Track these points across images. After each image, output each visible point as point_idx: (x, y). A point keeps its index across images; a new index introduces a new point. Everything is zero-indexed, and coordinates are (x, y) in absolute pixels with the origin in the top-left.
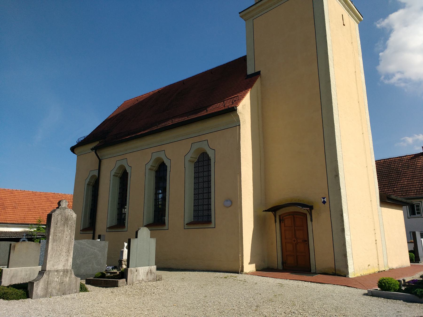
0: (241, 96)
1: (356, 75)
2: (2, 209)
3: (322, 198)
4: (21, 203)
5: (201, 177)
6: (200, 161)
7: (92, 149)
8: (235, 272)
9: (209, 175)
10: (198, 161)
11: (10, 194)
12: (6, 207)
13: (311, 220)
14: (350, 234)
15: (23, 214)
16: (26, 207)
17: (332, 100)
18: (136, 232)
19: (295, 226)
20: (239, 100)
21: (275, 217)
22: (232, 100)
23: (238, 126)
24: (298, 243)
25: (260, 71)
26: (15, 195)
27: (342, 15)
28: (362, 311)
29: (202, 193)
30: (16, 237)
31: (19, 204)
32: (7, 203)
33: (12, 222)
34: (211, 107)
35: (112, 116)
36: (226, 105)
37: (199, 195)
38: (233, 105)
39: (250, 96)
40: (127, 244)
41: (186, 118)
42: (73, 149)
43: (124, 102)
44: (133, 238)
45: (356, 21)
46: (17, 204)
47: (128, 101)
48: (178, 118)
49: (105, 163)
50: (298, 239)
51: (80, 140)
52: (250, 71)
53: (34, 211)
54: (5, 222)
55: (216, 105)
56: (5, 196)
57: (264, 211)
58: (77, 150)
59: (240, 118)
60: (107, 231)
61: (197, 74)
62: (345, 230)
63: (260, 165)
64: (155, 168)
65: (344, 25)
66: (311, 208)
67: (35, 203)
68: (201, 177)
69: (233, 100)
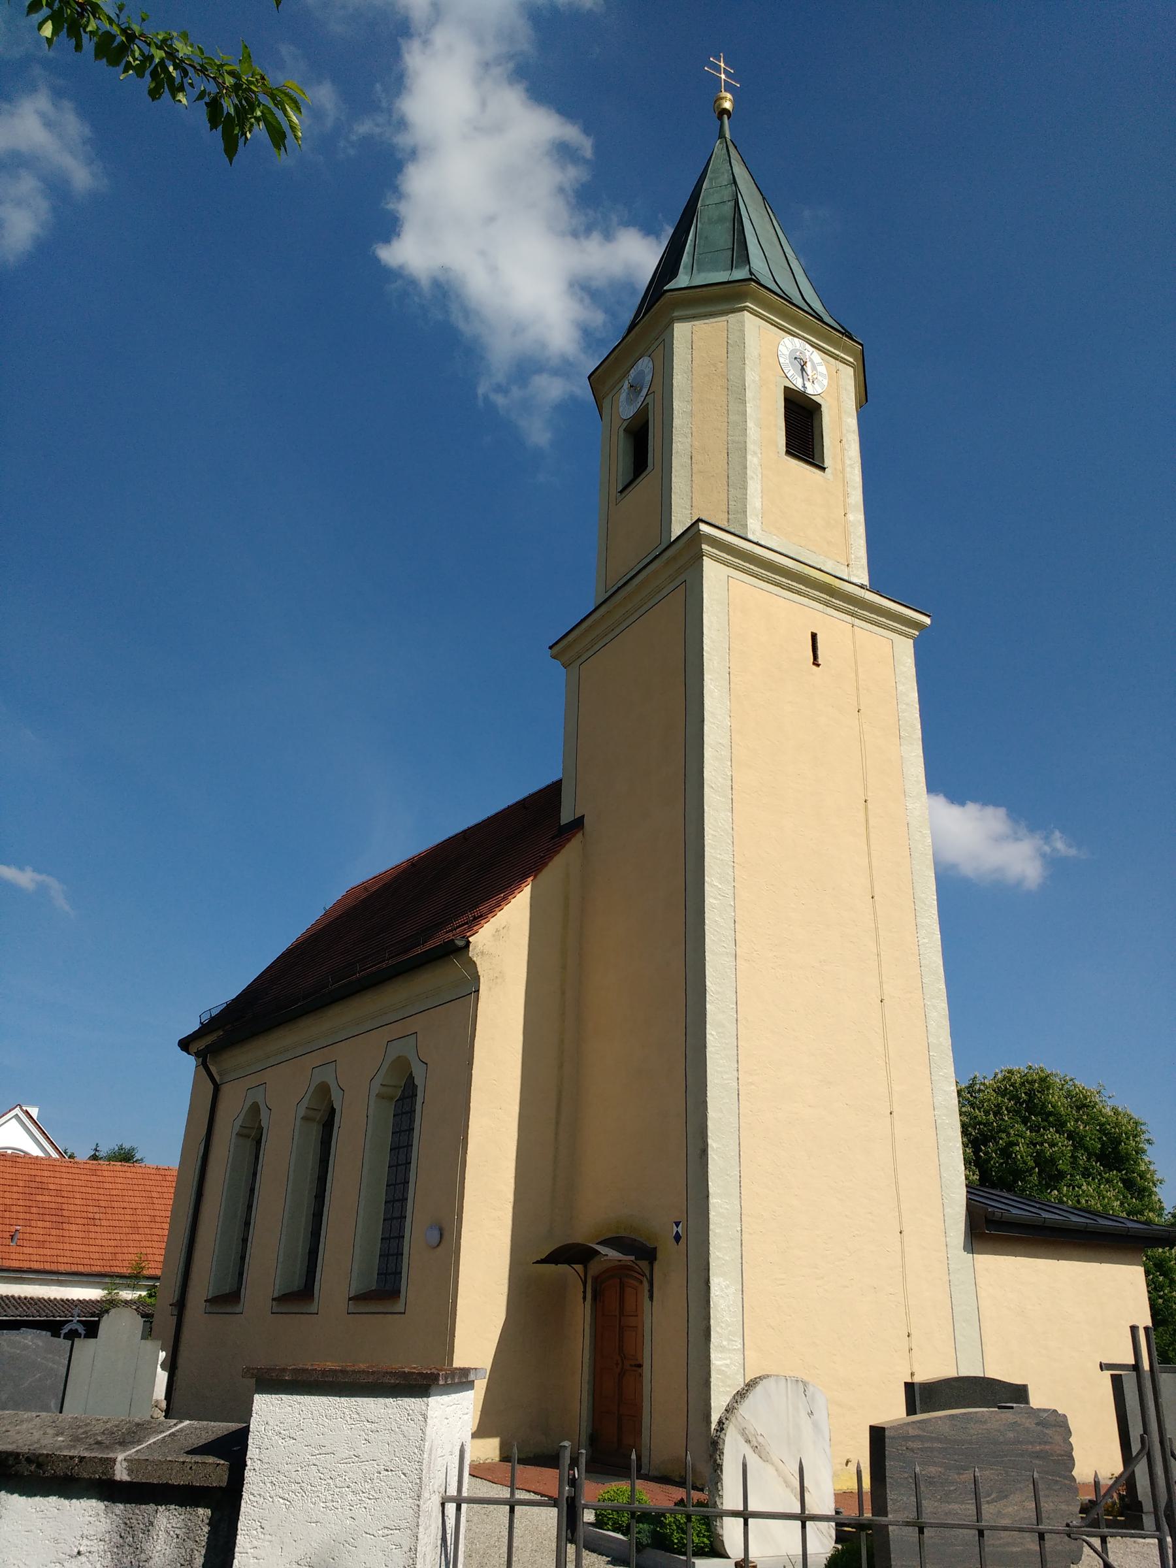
2: (54, 1225)
3: (675, 1222)
4: (115, 1204)
5: (404, 1147)
8: (1155, 1495)
11: (88, 1178)
12: (66, 1220)
13: (651, 1298)
14: (740, 1346)
15: (113, 1243)
16: (128, 1217)
17: (704, 913)
21: (585, 1284)
26: (101, 1179)
27: (814, 636)
28: (89, 1550)
30: (66, 1317)
31: (109, 1210)
32: (72, 1207)
33: (74, 1268)
39: (531, 897)
40: (164, 1353)
43: (347, 892)
45: (901, 633)
46: (103, 1210)
52: (566, 817)
53: (148, 1231)
54: (54, 1267)
56: (71, 1182)
59: (479, 969)
60: (207, 1311)
65: (818, 665)
66: (648, 1254)
67: (158, 1207)
69: (470, 916)
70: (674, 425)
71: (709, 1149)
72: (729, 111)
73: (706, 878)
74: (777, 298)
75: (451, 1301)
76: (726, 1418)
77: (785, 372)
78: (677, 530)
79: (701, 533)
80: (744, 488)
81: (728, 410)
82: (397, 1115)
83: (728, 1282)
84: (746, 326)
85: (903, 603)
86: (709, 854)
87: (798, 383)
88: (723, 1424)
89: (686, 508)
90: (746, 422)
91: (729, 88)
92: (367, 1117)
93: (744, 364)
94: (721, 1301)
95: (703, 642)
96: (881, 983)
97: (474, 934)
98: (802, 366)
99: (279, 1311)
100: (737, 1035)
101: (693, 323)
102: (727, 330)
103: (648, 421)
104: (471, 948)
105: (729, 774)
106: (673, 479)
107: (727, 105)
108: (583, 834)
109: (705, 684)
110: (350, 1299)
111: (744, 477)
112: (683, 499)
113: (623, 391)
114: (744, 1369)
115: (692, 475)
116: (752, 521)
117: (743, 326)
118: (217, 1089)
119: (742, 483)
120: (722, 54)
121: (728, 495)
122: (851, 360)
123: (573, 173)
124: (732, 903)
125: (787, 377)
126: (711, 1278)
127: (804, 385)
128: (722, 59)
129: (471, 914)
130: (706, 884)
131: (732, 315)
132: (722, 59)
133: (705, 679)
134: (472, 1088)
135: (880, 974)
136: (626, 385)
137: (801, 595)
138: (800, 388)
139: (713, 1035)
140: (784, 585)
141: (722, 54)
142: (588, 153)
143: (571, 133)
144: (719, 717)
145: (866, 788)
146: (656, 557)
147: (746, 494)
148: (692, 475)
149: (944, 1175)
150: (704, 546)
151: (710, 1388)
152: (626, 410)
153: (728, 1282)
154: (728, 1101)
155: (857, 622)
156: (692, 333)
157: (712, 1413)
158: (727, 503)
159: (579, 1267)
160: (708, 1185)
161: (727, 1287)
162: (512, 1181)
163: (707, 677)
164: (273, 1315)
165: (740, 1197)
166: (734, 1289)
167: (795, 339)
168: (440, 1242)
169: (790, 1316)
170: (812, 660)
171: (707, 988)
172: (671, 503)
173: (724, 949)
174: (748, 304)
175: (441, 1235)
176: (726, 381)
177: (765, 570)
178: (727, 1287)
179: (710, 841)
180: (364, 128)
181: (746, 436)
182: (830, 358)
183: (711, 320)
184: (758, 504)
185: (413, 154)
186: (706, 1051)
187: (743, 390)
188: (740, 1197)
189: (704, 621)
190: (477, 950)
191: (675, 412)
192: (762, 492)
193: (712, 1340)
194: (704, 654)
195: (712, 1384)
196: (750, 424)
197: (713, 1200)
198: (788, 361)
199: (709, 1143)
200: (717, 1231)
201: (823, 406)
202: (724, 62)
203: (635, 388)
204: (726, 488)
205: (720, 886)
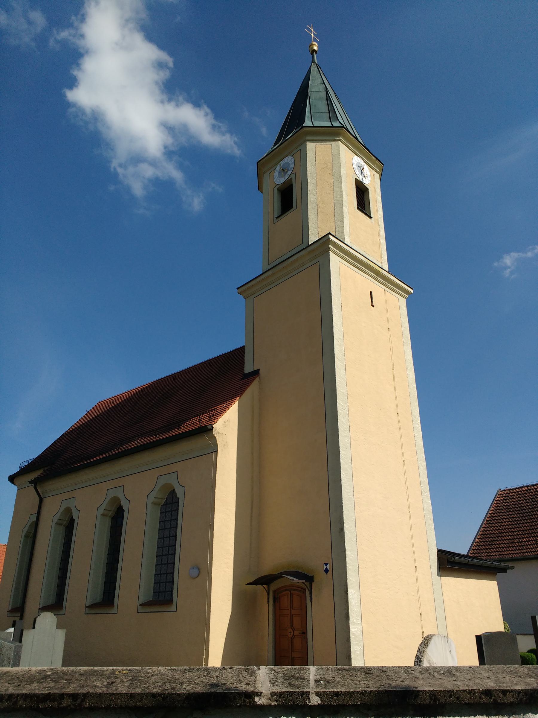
0: (225, 407)
1: (393, 373)
3: (324, 564)
5: (168, 528)
6: (168, 503)
7: (31, 482)
9: (171, 527)
10: (166, 504)
13: (311, 600)
14: (361, 622)
18: (34, 619)
19: (292, 609)
20: (218, 415)
21: (268, 594)
22: (200, 417)
23: (215, 452)
24: (295, 636)
25: (259, 369)
27: (371, 293)
29: (167, 555)
34: (183, 425)
35: (78, 425)
36: (202, 420)
37: (169, 557)
38: (210, 421)
41: (154, 439)
42: (12, 479)
43: (97, 403)
44: (29, 628)
45: (402, 296)
47: (116, 396)
48: (140, 439)
49: (47, 502)
50: (295, 630)
51: (23, 465)
52: (248, 369)
55: (194, 419)
57: (248, 584)
58: (17, 480)
59: (217, 441)
61: (194, 364)
62: (350, 616)
63: (252, 508)
64: (110, 514)
65: (373, 306)
66: (310, 579)
68: (168, 528)
69: (211, 415)
70: (308, 189)
71: (345, 528)
72: (316, 51)
73: (337, 400)
74: (352, 137)
75: (207, 604)
76: (421, 656)
77: (356, 171)
78: (313, 239)
79: (330, 239)
80: (343, 222)
81: (333, 185)
82: (162, 513)
83: (355, 592)
84: (340, 148)
85: (403, 281)
86: (338, 389)
87: (360, 178)
88: (421, 659)
89: (315, 228)
90: (342, 192)
91: (315, 41)
92: (146, 513)
93: (340, 165)
94: (353, 601)
95: (331, 290)
96: (403, 453)
97: (215, 423)
98: (361, 170)
99: (10, 616)
100: (352, 475)
101: (316, 143)
102: (332, 149)
103: (292, 185)
104: (214, 430)
105: (344, 353)
106: (309, 214)
107: (316, 48)
108: (259, 378)
109: (333, 310)
110: (39, 609)
111: (342, 217)
112: (314, 224)
113: (276, 171)
114: (362, 633)
115: (318, 213)
116: (346, 237)
117: (339, 148)
118: (41, 500)
119: (342, 219)
120: (312, 25)
121: (335, 224)
122: (379, 171)
123: (165, 75)
124: (348, 413)
125: (356, 174)
126: (348, 590)
127: (362, 179)
128: (312, 27)
129: (211, 413)
130: (338, 403)
131: (334, 142)
132: (312, 27)
133: (333, 308)
134: (215, 499)
135: (402, 449)
136: (278, 168)
137: (366, 274)
138: (361, 180)
139: (343, 474)
140: (360, 268)
141: (312, 25)
142: (171, 65)
143: (164, 56)
144: (339, 326)
145: (393, 364)
146: (303, 249)
147: (344, 225)
148: (318, 213)
149: (429, 541)
150: (330, 246)
151: (350, 642)
152: (278, 179)
153: (355, 592)
154: (351, 506)
155: (387, 289)
156: (315, 148)
157: (352, 655)
158: (335, 228)
159: (265, 586)
160: (345, 545)
161: (354, 594)
162: (233, 545)
163: (333, 307)
164: (85, 615)
165: (357, 551)
166: (357, 595)
167: (358, 157)
168: (198, 575)
169: (378, 607)
170: (371, 304)
171: (340, 452)
172: (308, 225)
173: (346, 434)
174: (341, 138)
175: (199, 572)
176: (332, 172)
177: (353, 261)
178: (354, 594)
179: (338, 383)
180: (64, 34)
181: (343, 198)
182: (371, 169)
183: (324, 143)
184: (348, 230)
185: (87, 52)
186: (341, 482)
187: (340, 177)
188: (357, 551)
189: (331, 281)
190: (216, 431)
191: (309, 183)
192: (349, 225)
193: (350, 619)
194: (332, 296)
195: (351, 640)
196: (344, 193)
197: (348, 553)
198: (356, 167)
199: (345, 526)
200: (349, 567)
201: (369, 189)
202: (313, 28)
203: (284, 170)
204: (334, 221)
205: (343, 405)
